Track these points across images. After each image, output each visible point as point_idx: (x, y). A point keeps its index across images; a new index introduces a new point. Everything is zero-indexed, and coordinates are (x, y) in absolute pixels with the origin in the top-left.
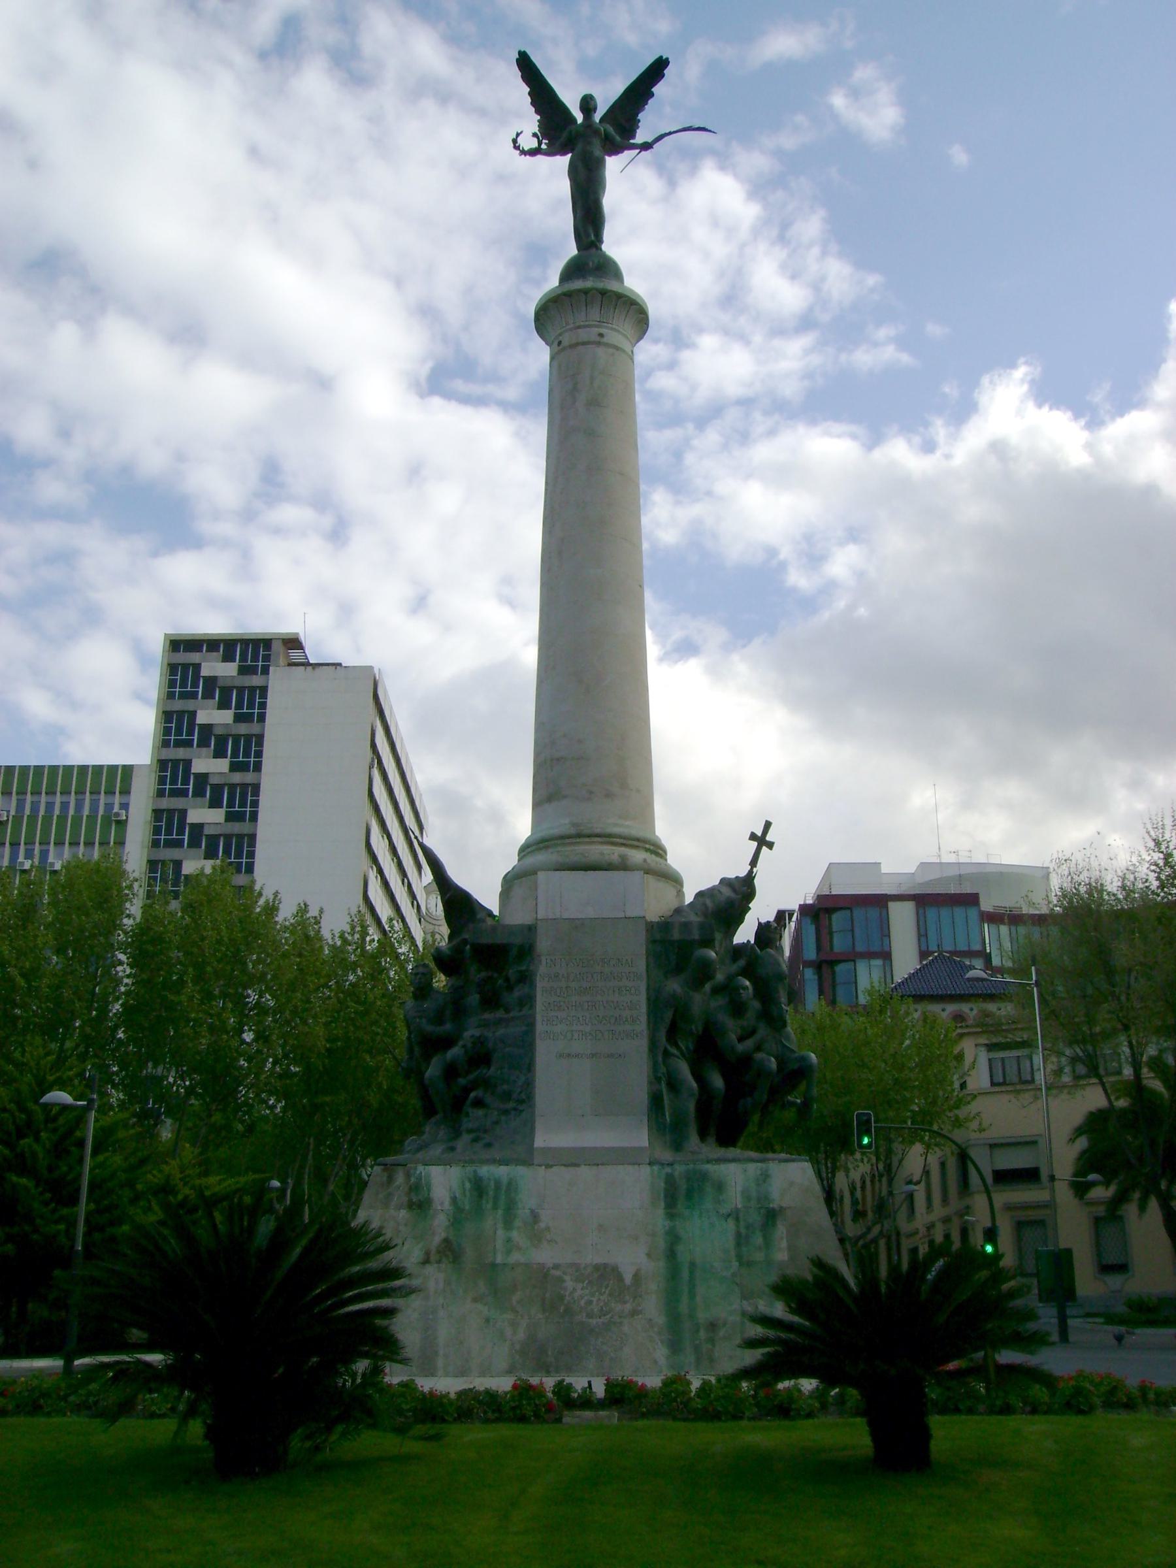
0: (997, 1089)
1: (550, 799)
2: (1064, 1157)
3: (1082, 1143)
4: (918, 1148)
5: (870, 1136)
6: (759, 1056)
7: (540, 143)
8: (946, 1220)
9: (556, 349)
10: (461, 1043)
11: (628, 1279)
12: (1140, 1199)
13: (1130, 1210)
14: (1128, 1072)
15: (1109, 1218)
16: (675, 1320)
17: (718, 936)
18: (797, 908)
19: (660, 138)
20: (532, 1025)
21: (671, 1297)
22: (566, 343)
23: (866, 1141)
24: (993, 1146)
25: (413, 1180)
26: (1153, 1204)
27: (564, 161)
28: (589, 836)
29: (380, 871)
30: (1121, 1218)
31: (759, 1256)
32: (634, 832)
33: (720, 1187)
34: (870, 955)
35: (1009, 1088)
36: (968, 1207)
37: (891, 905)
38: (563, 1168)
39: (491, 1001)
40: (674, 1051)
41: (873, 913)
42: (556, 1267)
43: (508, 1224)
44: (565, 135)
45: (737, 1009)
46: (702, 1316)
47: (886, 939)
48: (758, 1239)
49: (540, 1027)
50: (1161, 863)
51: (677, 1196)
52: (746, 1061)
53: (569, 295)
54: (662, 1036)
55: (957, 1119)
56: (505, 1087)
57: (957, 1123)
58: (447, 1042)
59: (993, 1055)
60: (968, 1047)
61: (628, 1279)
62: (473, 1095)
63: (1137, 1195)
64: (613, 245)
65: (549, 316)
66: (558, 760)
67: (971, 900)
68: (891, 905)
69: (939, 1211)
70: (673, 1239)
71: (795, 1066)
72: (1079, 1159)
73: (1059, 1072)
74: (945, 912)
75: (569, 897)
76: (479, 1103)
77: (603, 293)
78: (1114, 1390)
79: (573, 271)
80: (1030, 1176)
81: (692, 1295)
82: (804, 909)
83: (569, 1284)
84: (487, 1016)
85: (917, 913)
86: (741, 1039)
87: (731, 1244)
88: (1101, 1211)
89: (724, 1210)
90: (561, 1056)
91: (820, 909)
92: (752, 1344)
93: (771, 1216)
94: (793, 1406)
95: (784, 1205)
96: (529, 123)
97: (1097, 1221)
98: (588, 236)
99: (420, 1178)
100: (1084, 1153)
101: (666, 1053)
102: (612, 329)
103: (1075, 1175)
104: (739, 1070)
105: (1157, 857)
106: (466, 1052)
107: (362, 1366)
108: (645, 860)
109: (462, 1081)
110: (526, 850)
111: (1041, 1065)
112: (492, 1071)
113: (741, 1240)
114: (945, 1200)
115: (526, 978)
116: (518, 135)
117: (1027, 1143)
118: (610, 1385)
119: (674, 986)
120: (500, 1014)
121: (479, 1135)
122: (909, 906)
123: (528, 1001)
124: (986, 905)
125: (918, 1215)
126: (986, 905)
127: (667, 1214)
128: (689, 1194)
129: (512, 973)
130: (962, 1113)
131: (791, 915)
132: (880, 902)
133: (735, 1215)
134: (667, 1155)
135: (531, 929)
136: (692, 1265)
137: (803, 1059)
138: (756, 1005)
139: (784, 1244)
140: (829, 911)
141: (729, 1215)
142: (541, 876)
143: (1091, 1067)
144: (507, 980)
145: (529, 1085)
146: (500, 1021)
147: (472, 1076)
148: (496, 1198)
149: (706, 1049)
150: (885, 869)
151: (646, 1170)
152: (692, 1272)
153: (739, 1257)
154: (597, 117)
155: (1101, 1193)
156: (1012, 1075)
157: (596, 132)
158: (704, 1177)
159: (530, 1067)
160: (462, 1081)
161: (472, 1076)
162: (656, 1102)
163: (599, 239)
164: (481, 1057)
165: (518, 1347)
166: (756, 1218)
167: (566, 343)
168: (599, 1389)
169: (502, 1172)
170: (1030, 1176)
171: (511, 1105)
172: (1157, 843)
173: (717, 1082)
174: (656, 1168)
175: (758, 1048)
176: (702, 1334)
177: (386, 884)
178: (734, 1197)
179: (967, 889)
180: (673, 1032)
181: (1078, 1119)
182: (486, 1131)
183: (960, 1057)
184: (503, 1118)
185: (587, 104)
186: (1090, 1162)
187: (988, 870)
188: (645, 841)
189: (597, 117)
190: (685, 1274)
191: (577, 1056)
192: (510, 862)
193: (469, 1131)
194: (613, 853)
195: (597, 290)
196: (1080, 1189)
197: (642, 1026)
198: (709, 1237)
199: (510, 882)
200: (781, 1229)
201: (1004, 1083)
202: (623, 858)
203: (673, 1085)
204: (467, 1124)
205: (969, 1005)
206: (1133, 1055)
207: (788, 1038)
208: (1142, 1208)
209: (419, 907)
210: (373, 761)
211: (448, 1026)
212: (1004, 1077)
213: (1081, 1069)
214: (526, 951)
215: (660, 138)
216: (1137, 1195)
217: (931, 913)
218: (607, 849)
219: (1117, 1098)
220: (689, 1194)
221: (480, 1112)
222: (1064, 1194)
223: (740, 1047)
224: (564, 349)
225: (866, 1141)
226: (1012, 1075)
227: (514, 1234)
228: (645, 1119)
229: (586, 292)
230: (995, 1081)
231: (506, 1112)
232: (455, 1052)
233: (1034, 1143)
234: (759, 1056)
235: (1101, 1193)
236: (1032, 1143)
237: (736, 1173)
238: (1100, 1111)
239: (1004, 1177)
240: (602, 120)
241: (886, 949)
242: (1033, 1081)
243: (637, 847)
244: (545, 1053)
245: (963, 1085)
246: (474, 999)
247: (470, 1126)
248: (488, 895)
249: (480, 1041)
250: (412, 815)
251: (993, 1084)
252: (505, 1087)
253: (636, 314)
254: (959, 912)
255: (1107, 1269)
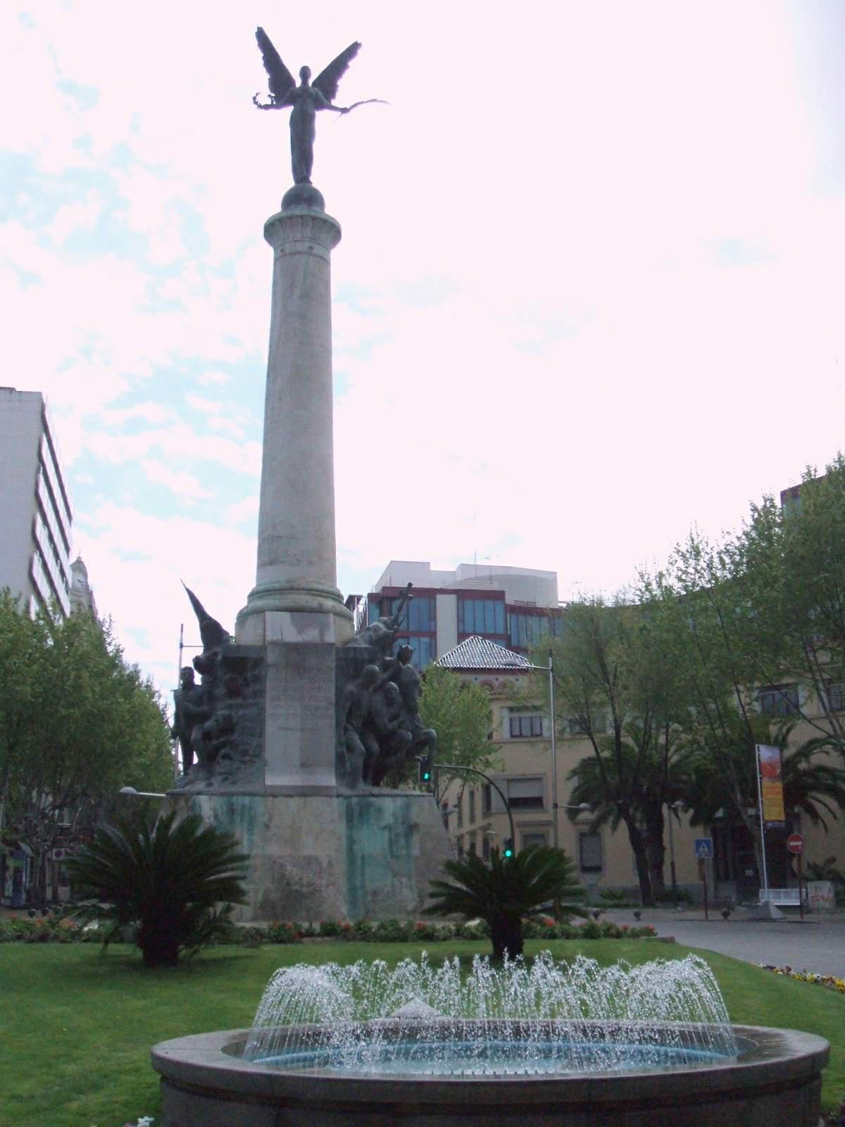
0: (516, 740)
1: (271, 563)
2: (564, 791)
3: (575, 782)
4: (458, 782)
5: (429, 774)
6: (403, 732)
7: (272, 102)
8: (473, 834)
9: (280, 254)
10: (214, 718)
11: (325, 864)
12: (613, 822)
13: (606, 829)
14: (611, 732)
15: (591, 834)
16: (352, 889)
17: (379, 655)
18: (365, 595)
19: (355, 105)
20: (262, 710)
21: (351, 875)
22: (287, 251)
23: (426, 776)
24: (510, 781)
25: (190, 804)
26: (623, 824)
27: (288, 111)
28: (298, 589)
29: (42, 555)
30: (599, 834)
31: (404, 852)
32: (326, 588)
33: (380, 811)
34: (419, 634)
35: (526, 740)
36: (490, 824)
37: (439, 597)
38: (284, 798)
39: (233, 692)
40: (350, 727)
41: (423, 603)
42: (281, 857)
43: (250, 831)
44: (288, 94)
45: (389, 701)
46: (369, 887)
47: (433, 623)
48: (402, 842)
49: (269, 710)
50: (643, 590)
51: (356, 815)
52: (393, 733)
53: (290, 218)
54: (344, 718)
55: (487, 762)
56: (243, 747)
57: (487, 764)
58: (204, 717)
59: (516, 715)
60: (495, 707)
61: (325, 864)
62: (223, 751)
63: (611, 819)
64: (318, 179)
65: (273, 230)
66: (278, 537)
67: (498, 596)
68: (439, 597)
69: (467, 826)
70: (351, 842)
71: (423, 738)
72: (573, 793)
73: (562, 731)
74: (479, 604)
75: (282, 628)
76: (227, 757)
77: (314, 219)
78: (609, 929)
79: (291, 199)
80: (536, 803)
81: (363, 874)
82: (371, 596)
83: (289, 868)
84: (230, 702)
85: (458, 605)
86: (390, 721)
87: (386, 846)
88: (586, 829)
89: (383, 824)
90: (281, 729)
91: (383, 598)
92: (433, 895)
93: (412, 828)
94: (436, 934)
95: (418, 822)
96: (262, 79)
97: (582, 836)
98: (302, 173)
99: (194, 802)
100: (576, 790)
101: (346, 730)
102: (319, 244)
103: (570, 803)
104: (386, 739)
105: (642, 585)
106: (218, 724)
107: (220, 906)
108: (333, 607)
109: (215, 742)
110: (253, 595)
111: (549, 726)
112: (235, 736)
113: (392, 842)
114: (472, 819)
115: (258, 679)
116: (257, 94)
117: (536, 779)
118: (322, 924)
119: (351, 687)
120: (240, 701)
121: (227, 777)
122: (453, 597)
123: (260, 693)
124: (510, 599)
125: (451, 828)
126: (510, 599)
127: (347, 826)
128: (361, 815)
129: (249, 675)
130: (491, 758)
131: (359, 598)
132: (430, 594)
133: (389, 828)
134: (345, 791)
135: (263, 648)
136: (363, 858)
137: (427, 734)
138: (400, 699)
139: (418, 845)
140: (392, 599)
141: (385, 828)
142: (268, 614)
143: (585, 727)
144: (245, 679)
145: (261, 748)
146: (241, 706)
147: (222, 740)
148: (242, 815)
149: (369, 725)
150: (433, 568)
151: (336, 802)
152: (363, 863)
153: (391, 852)
154: (310, 82)
155: (586, 816)
156: (526, 731)
157: (310, 95)
158: (369, 805)
159: (262, 734)
160: (215, 742)
161: (222, 740)
162: (340, 759)
163: (308, 170)
164: (227, 728)
165: (258, 905)
166: (401, 829)
167: (287, 251)
168: (317, 927)
169: (247, 800)
170: (536, 803)
171: (248, 758)
172: (642, 576)
173: (375, 747)
174: (340, 799)
175: (400, 726)
176: (370, 898)
177: (45, 565)
178: (388, 819)
179: (496, 587)
180: (350, 714)
181: (574, 764)
182: (231, 774)
183: (489, 717)
184: (243, 766)
185: (305, 72)
186: (581, 795)
187: (512, 573)
188: (333, 593)
189: (310, 82)
190: (359, 863)
191: (291, 729)
192: (242, 603)
193: (220, 774)
194: (314, 602)
195: (311, 216)
196: (573, 813)
197: (332, 712)
198: (373, 841)
199: (243, 617)
200: (416, 838)
201: (521, 735)
202: (321, 605)
203: (350, 748)
204: (218, 769)
205: (496, 676)
206: (616, 720)
207: (418, 721)
208: (614, 828)
209: (67, 582)
210: (39, 469)
211: (205, 708)
212: (520, 730)
213: (577, 728)
214: (259, 662)
215: (355, 105)
216: (611, 819)
217: (469, 604)
218: (309, 598)
219: (603, 751)
220: (361, 815)
221: (228, 762)
222: (562, 816)
223: (390, 726)
224: (285, 255)
225: (426, 776)
226: (526, 731)
227: (255, 838)
228: (333, 769)
229: (302, 217)
230: (514, 734)
231: (245, 762)
232: (208, 724)
233: (540, 779)
234: (403, 732)
235: (586, 816)
236: (538, 779)
237: (389, 804)
238: (590, 759)
239: (515, 804)
240: (314, 84)
241: (433, 629)
242: (541, 734)
243: (326, 597)
244: (271, 727)
245: (490, 736)
246: (220, 691)
247: (221, 770)
248: (229, 625)
249: (228, 719)
250: (65, 511)
251: (512, 736)
252: (243, 747)
253: (332, 231)
254: (489, 604)
255: (586, 869)
